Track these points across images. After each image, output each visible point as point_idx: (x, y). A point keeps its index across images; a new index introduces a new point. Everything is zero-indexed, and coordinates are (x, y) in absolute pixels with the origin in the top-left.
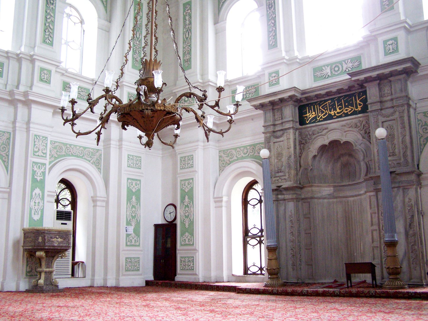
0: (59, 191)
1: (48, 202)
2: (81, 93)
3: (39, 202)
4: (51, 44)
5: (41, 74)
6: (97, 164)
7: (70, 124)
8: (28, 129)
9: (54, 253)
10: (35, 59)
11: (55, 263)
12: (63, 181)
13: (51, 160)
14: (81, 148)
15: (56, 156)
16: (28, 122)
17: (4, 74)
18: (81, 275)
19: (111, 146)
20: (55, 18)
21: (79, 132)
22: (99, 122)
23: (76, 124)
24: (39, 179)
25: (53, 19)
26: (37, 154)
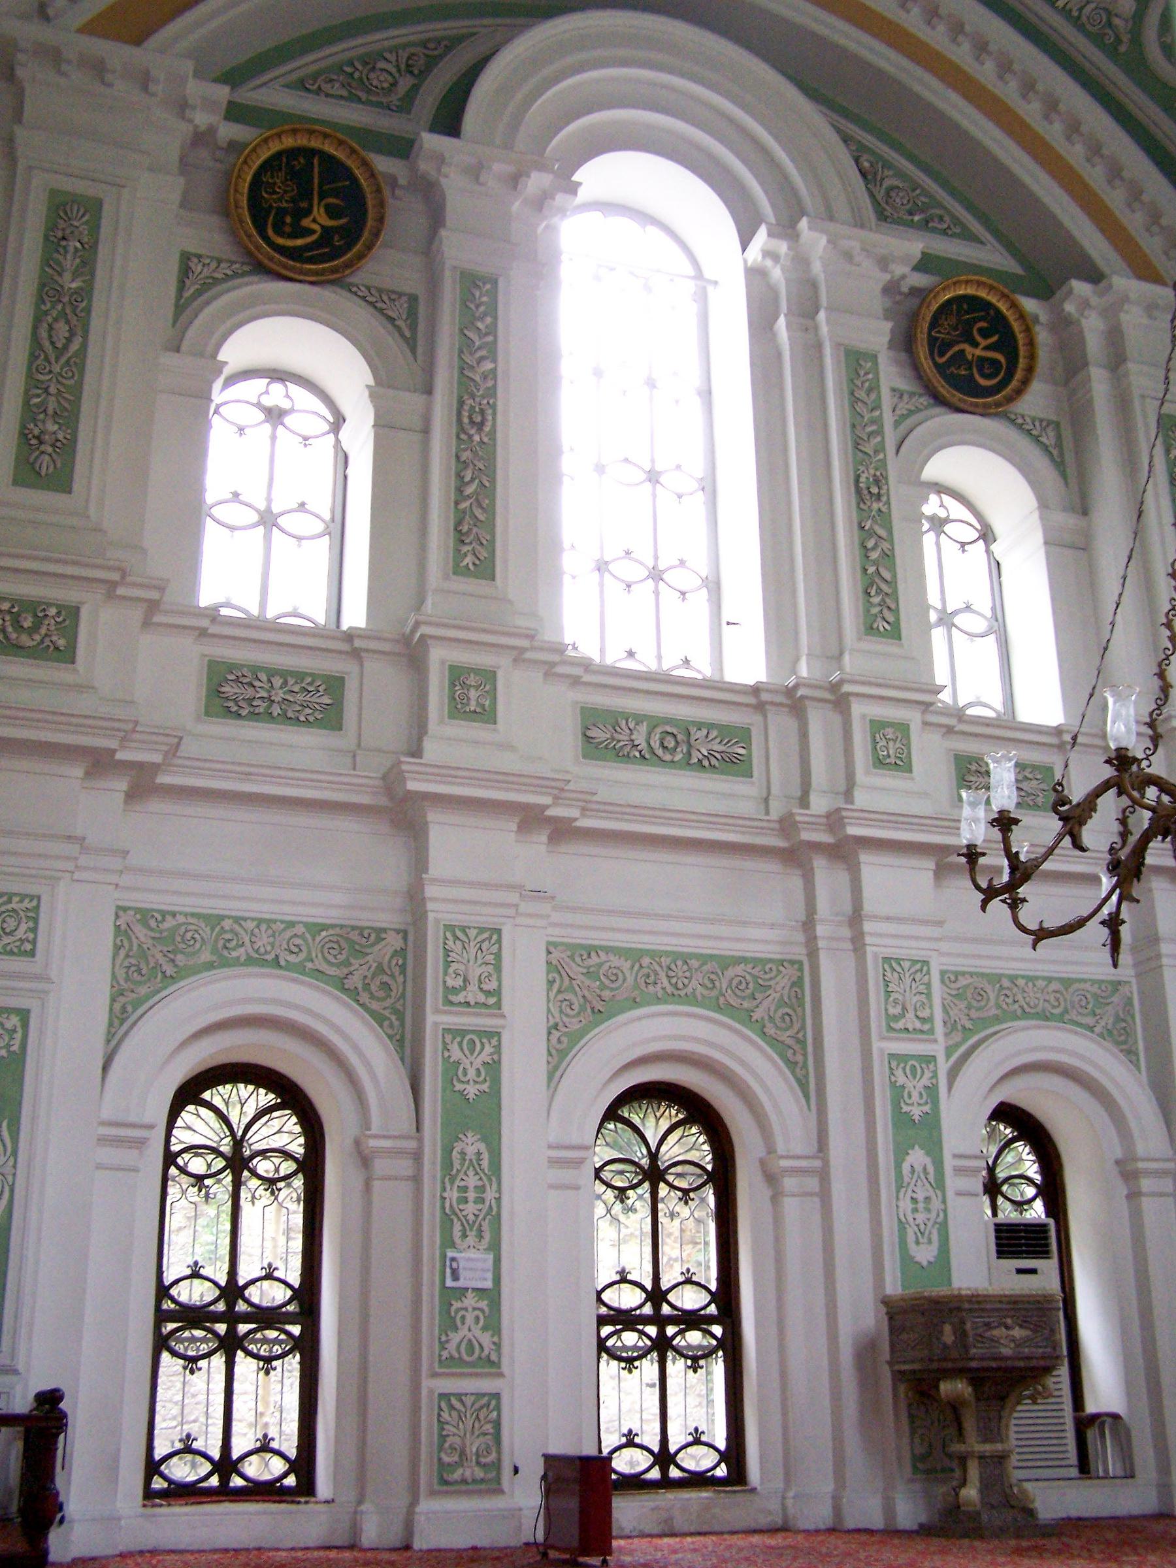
0: (994, 1150)
1: (959, 1194)
2: (1024, 785)
3: (927, 1199)
4: (895, 633)
5: (875, 742)
6: (1119, 1037)
7: (1003, 901)
8: (858, 942)
9: (1006, 1383)
10: (849, 694)
11: (1014, 1422)
12: (1005, 1113)
13: (951, 1042)
14: (1054, 986)
15: (968, 1025)
16: (856, 918)
17: (755, 761)
18: (1113, 1465)
19: (1165, 961)
20: (892, 544)
21: (1041, 929)
22: (1107, 882)
23: (1024, 900)
24: (916, 1112)
25: (885, 545)
26: (900, 1025)
